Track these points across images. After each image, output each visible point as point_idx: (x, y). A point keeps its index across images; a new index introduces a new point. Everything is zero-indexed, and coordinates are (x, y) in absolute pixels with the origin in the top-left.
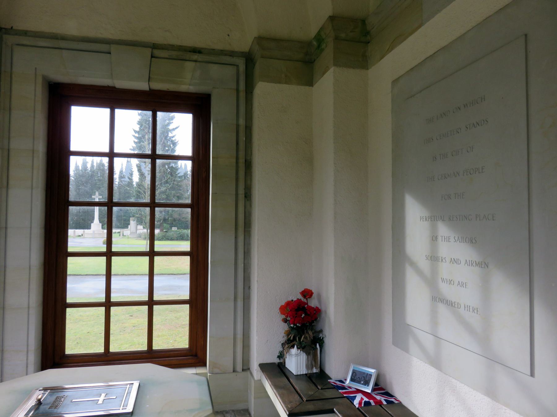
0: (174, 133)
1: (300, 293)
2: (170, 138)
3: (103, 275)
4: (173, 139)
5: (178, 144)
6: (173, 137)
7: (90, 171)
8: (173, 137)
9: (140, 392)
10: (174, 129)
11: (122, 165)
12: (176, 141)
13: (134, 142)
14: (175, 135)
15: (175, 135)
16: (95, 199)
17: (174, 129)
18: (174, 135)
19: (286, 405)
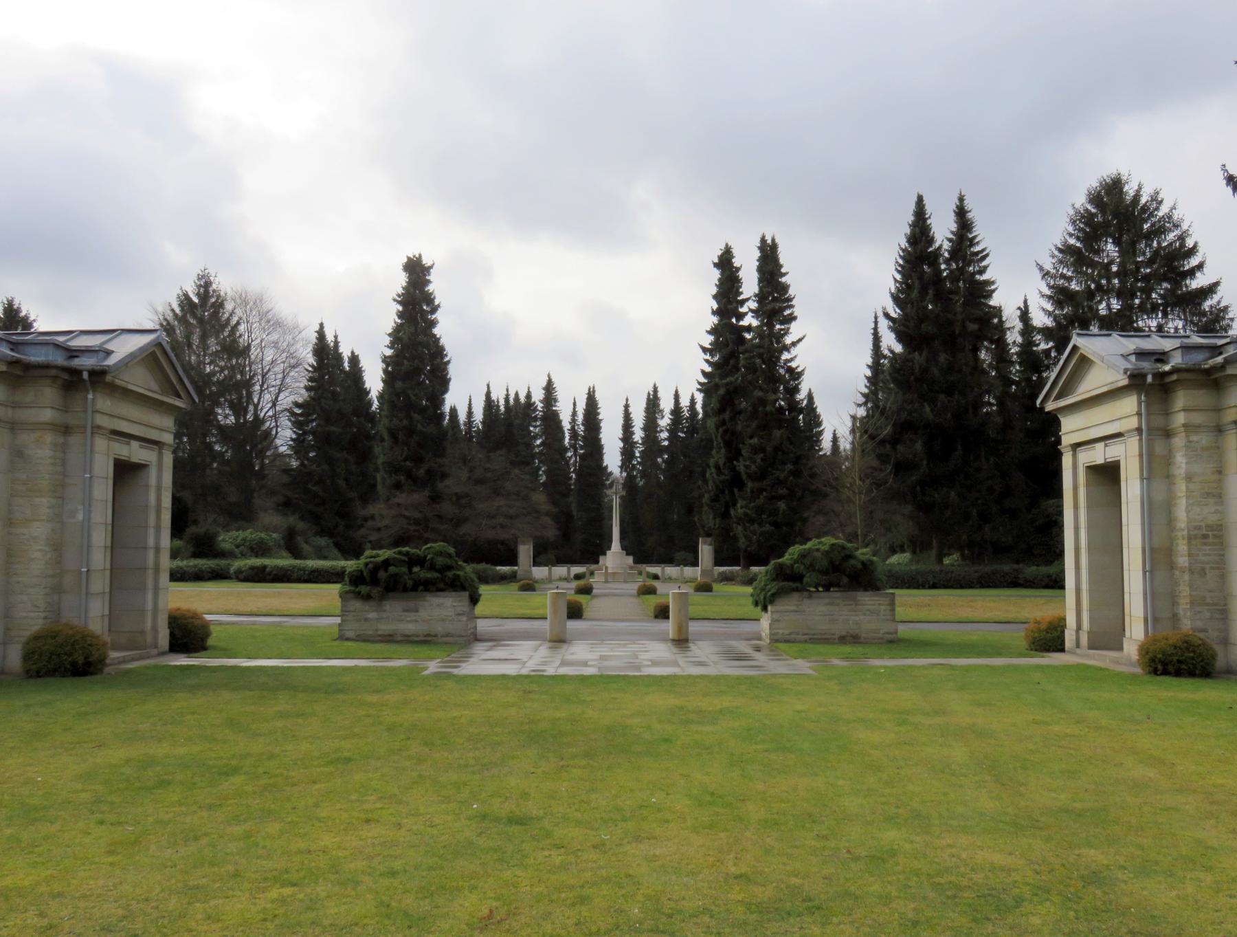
0: (794, 351)
1: (1114, 187)
2: (785, 364)
3: (170, 432)
4: (793, 364)
5: (1232, 320)
6: (791, 360)
7: (1062, 309)
8: (791, 360)
9: (324, 612)
10: (794, 344)
11: (575, 404)
12: (799, 370)
13: (704, 373)
14: (795, 357)
15: (795, 357)
16: (1094, 326)
17: (794, 344)
18: (792, 356)
19: (765, 290)
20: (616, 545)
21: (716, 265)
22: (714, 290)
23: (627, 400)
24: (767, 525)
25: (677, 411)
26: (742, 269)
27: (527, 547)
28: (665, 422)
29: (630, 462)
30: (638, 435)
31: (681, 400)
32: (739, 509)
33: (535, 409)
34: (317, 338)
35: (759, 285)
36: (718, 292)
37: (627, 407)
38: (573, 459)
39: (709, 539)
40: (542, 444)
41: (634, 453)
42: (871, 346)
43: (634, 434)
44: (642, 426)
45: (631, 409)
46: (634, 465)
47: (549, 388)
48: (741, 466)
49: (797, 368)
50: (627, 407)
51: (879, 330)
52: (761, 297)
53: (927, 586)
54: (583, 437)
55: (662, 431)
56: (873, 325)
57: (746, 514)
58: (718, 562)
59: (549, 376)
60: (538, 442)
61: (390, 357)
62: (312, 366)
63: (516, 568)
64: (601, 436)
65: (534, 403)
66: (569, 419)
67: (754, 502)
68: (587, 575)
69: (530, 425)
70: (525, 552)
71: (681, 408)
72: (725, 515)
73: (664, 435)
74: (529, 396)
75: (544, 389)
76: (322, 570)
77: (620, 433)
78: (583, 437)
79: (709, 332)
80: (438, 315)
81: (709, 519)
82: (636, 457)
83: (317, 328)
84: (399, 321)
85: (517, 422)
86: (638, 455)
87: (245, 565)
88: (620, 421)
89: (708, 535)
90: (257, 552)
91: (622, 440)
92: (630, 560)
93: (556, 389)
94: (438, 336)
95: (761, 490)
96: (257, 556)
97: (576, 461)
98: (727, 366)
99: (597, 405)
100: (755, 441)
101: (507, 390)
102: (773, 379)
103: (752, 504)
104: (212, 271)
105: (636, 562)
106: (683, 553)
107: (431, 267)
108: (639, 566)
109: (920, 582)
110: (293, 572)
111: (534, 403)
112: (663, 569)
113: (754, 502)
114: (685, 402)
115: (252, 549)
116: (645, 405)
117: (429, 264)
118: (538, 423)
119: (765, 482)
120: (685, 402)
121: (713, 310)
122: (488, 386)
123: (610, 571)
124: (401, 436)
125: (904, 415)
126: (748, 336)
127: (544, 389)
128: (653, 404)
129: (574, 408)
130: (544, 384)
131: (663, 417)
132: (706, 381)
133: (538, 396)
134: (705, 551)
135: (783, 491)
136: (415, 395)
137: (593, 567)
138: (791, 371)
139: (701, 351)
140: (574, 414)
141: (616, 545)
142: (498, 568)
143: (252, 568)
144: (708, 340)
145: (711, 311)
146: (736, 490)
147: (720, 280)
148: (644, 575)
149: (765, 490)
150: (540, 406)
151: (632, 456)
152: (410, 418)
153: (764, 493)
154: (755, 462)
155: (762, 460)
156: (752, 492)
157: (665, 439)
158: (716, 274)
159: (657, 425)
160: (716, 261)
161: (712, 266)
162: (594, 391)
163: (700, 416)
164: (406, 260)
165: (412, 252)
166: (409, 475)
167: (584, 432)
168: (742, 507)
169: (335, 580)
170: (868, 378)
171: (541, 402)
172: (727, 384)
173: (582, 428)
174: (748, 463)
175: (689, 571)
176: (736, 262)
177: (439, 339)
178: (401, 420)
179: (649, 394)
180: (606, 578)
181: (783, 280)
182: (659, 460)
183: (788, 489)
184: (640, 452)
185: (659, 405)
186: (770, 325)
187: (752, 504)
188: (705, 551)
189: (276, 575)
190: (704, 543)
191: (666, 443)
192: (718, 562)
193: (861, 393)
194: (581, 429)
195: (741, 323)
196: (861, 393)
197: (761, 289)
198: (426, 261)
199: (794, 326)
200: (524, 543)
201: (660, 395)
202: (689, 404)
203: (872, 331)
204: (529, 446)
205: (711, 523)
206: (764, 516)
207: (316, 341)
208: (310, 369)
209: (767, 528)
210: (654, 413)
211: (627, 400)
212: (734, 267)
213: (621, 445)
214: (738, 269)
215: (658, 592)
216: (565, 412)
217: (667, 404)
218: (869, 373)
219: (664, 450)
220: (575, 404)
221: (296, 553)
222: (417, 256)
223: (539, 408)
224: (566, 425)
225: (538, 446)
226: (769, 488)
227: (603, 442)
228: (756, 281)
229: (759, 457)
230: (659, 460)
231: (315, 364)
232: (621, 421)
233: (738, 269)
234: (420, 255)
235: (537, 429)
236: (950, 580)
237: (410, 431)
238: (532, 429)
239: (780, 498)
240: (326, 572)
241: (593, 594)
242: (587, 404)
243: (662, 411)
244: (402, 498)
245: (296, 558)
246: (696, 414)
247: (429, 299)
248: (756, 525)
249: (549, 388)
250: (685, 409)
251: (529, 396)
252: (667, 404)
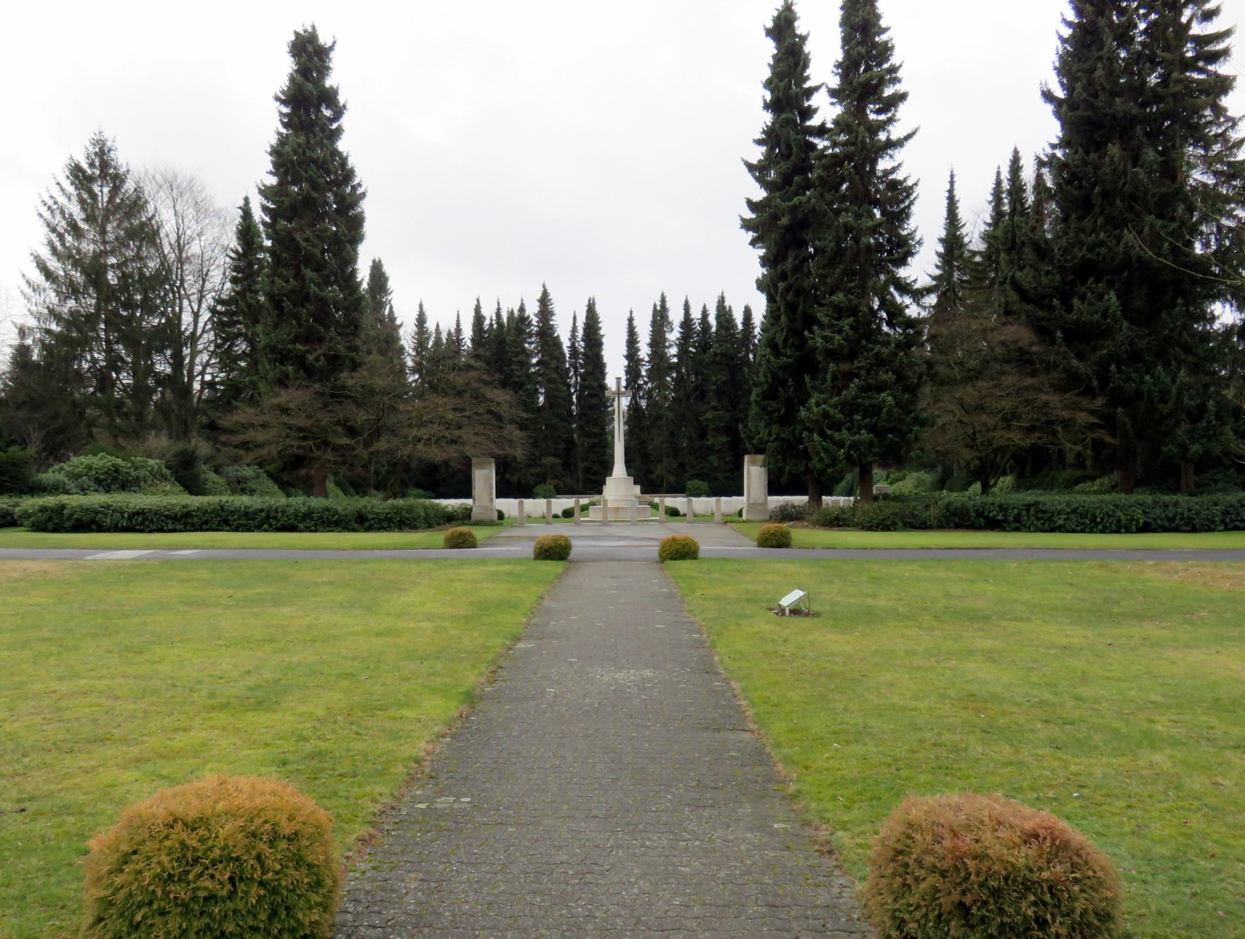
0: (899, 155)
4: (899, 176)
6: (894, 170)
8: (894, 170)
11: (575, 318)
12: (909, 183)
15: (900, 165)
17: (899, 143)
18: (895, 164)
20: (619, 468)
21: (769, 33)
22: (767, 74)
23: (631, 312)
24: (863, 431)
25: (687, 324)
26: (810, 38)
27: (485, 472)
28: (674, 335)
29: (636, 382)
30: (644, 352)
31: (692, 311)
32: (814, 407)
33: (530, 324)
34: (242, 217)
35: (843, 47)
36: (793, 29)
37: (631, 320)
38: (574, 379)
39: (760, 457)
40: (538, 363)
41: (640, 371)
42: (945, 214)
43: (639, 350)
44: (648, 341)
45: (635, 323)
46: (640, 386)
47: (544, 300)
48: (817, 339)
49: (905, 180)
50: (631, 320)
51: (955, 192)
52: (848, 67)
53: (1134, 528)
54: (584, 354)
55: (671, 346)
56: (948, 187)
57: (826, 415)
58: (775, 487)
59: (544, 286)
60: (534, 361)
61: (272, 187)
62: (236, 252)
63: (469, 502)
64: (603, 353)
65: (529, 317)
66: (569, 335)
67: (839, 394)
68: (577, 512)
69: (524, 341)
70: (484, 477)
71: (692, 320)
72: (788, 419)
73: (674, 351)
74: (522, 309)
75: (539, 301)
76: (150, 510)
77: (624, 351)
78: (584, 354)
79: (759, 142)
80: (345, 121)
81: (756, 425)
82: (642, 376)
83: (242, 203)
84: (284, 131)
85: (509, 339)
86: (644, 373)
87: (33, 506)
88: (624, 336)
89: (759, 451)
90: (109, 486)
91: (627, 357)
92: (637, 489)
93: (552, 301)
94: (345, 154)
95: (850, 376)
96: (108, 490)
97: (576, 382)
98: (790, 185)
99: (598, 318)
100: (840, 297)
101: (498, 304)
102: (863, 198)
103: (836, 399)
104: (107, 135)
105: (642, 492)
106: (696, 481)
107: (331, 48)
108: (647, 496)
109: (1124, 521)
110: (106, 515)
111: (529, 317)
112: (690, 502)
113: (839, 394)
114: (696, 314)
115: (99, 481)
116: (651, 318)
117: (329, 44)
118: (533, 339)
119: (856, 363)
120: (696, 314)
121: (765, 101)
122: (478, 300)
123: (610, 505)
124: (287, 304)
125: (1080, 253)
126: (821, 143)
127: (539, 301)
128: (660, 318)
129: (574, 323)
130: (539, 295)
131: (672, 330)
132: (753, 216)
133: (532, 310)
134: (754, 473)
135: (887, 377)
136: (307, 240)
137: (596, 498)
138: (894, 185)
139: (745, 169)
140: (574, 329)
141: (619, 468)
142: (437, 501)
143: (43, 509)
144: (757, 154)
145: (762, 104)
146: (807, 378)
147: (774, 57)
148: (662, 511)
149: (858, 376)
150: (535, 320)
151: (638, 375)
152: (298, 275)
153: (856, 380)
154: (840, 332)
155: (852, 327)
156: (835, 379)
157: (674, 356)
158: (769, 48)
159: (665, 340)
160: (770, 25)
161: (763, 33)
162: (594, 304)
163: (714, 329)
164: (293, 38)
165: (301, 25)
166: (300, 362)
167: (584, 348)
168: (818, 405)
169: (170, 527)
170: (939, 255)
171: (536, 315)
172: (794, 209)
173: (582, 344)
174: (827, 333)
175: (730, 504)
176: (801, 28)
177: (346, 158)
178: (287, 281)
179: (655, 305)
180: (605, 515)
181: (884, 37)
182: (668, 379)
183: (894, 373)
184: (647, 371)
185: (667, 317)
186: (860, 111)
187: (836, 399)
188: (754, 473)
189: (78, 520)
190: (753, 463)
191: (675, 360)
192: (775, 487)
193: (930, 276)
194: (581, 346)
195: (808, 123)
196: (930, 276)
197: (847, 54)
198: (324, 39)
199: (902, 110)
200: (481, 466)
201: (668, 305)
202: (700, 316)
203: (947, 194)
204: (525, 364)
205: (763, 434)
206: (857, 417)
207: (240, 220)
208: (233, 255)
209: (865, 435)
210: (662, 326)
211: (631, 312)
212: (796, 36)
213: (626, 363)
214: (803, 39)
215: (700, 555)
216: (563, 333)
217: (676, 316)
218: (941, 249)
219: (672, 367)
220: (575, 318)
221: (193, 487)
222: (310, 29)
223: (534, 323)
224: (566, 344)
225: (534, 365)
226: (863, 372)
227: (605, 360)
228: (839, 43)
229: (846, 323)
230: (668, 379)
231: (240, 250)
232: (625, 337)
233: (803, 39)
234: (313, 27)
235: (533, 346)
236: (1172, 520)
237: (303, 297)
238: (526, 345)
239: (881, 388)
240: (156, 513)
241: (570, 557)
242: (587, 318)
243: (670, 323)
244: (284, 397)
245: (192, 493)
246: (709, 327)
247: (329, 97)
248: (844, 431)
249: (544, 300)
250: (697, 322)
251: (522, 309)
252: (676, 316)
